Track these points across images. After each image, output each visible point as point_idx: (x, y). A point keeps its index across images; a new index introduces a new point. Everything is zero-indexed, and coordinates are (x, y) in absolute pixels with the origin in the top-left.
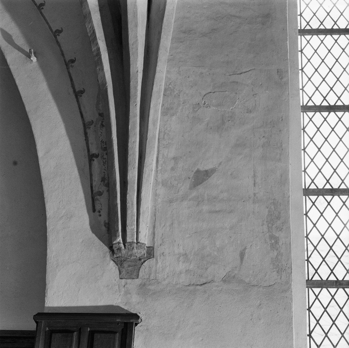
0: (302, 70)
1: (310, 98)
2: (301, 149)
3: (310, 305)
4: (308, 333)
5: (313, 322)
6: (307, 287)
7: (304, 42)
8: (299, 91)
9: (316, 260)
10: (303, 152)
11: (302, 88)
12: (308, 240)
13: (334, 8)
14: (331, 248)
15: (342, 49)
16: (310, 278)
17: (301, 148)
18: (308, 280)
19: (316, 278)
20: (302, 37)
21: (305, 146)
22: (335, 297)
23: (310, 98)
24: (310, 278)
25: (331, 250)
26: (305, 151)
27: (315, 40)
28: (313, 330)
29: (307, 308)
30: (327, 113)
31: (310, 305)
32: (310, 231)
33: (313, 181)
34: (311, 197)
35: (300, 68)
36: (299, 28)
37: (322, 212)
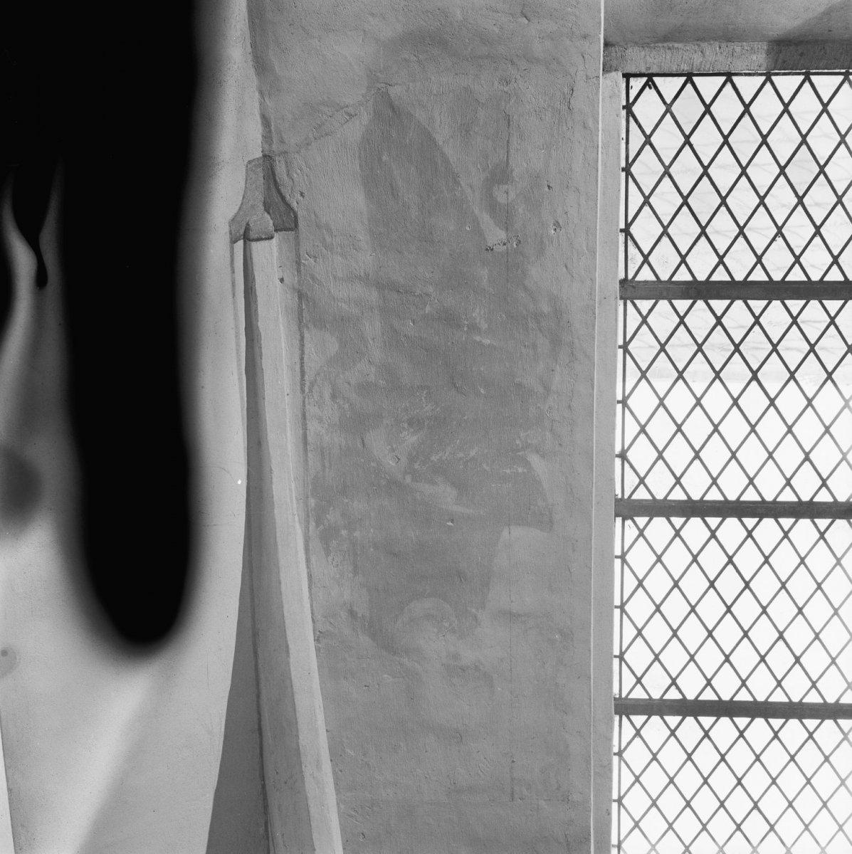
0: (622, 607)
1: (642, 481)
2: (612, 653)
3: (630, 219)
4: (622, 226)
5: (637, 139)
6: (621, 298)
7: (628, 731)
8: (611, 804)
9: (645, 230)
10: (619, 406)
11: (624, 227)
12: (627, 340)
13: (690, 842)
14: (682, 321)
15: (710, 739)
16: (630, 277)
17: (614, 394)
18: (624, 282)
19: (646, 275)
20: (624, 718)
21: (623, 747)
22: (688, 259)
23: (639, 681)
24: (630, 277)
25: (682, 314)
26: (626, 351)
27: (655, 728)
28: (626, 793)
29: (623, 164)
30: (683, 519)
31: (628, 338)
32: (626, 789)
33: (642, 481)
34: (633, 718)
35: (617, 652)
36: (620, 496)
37: (661, 409)
